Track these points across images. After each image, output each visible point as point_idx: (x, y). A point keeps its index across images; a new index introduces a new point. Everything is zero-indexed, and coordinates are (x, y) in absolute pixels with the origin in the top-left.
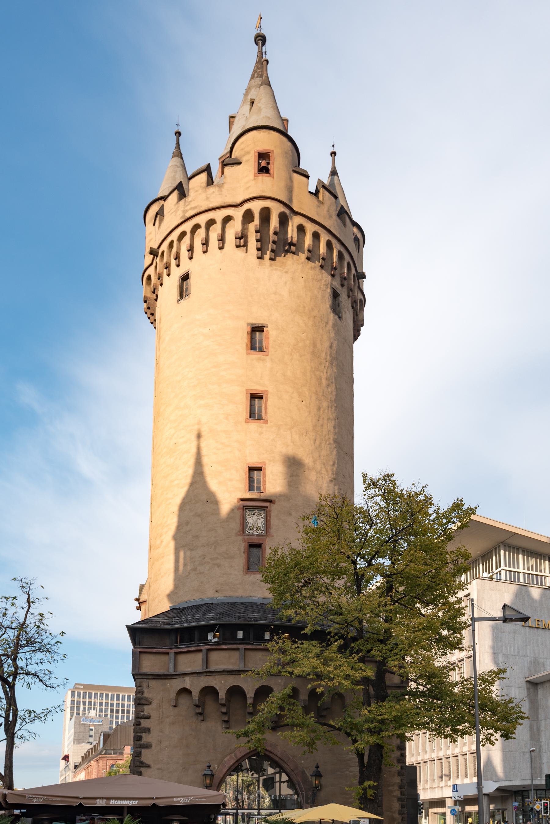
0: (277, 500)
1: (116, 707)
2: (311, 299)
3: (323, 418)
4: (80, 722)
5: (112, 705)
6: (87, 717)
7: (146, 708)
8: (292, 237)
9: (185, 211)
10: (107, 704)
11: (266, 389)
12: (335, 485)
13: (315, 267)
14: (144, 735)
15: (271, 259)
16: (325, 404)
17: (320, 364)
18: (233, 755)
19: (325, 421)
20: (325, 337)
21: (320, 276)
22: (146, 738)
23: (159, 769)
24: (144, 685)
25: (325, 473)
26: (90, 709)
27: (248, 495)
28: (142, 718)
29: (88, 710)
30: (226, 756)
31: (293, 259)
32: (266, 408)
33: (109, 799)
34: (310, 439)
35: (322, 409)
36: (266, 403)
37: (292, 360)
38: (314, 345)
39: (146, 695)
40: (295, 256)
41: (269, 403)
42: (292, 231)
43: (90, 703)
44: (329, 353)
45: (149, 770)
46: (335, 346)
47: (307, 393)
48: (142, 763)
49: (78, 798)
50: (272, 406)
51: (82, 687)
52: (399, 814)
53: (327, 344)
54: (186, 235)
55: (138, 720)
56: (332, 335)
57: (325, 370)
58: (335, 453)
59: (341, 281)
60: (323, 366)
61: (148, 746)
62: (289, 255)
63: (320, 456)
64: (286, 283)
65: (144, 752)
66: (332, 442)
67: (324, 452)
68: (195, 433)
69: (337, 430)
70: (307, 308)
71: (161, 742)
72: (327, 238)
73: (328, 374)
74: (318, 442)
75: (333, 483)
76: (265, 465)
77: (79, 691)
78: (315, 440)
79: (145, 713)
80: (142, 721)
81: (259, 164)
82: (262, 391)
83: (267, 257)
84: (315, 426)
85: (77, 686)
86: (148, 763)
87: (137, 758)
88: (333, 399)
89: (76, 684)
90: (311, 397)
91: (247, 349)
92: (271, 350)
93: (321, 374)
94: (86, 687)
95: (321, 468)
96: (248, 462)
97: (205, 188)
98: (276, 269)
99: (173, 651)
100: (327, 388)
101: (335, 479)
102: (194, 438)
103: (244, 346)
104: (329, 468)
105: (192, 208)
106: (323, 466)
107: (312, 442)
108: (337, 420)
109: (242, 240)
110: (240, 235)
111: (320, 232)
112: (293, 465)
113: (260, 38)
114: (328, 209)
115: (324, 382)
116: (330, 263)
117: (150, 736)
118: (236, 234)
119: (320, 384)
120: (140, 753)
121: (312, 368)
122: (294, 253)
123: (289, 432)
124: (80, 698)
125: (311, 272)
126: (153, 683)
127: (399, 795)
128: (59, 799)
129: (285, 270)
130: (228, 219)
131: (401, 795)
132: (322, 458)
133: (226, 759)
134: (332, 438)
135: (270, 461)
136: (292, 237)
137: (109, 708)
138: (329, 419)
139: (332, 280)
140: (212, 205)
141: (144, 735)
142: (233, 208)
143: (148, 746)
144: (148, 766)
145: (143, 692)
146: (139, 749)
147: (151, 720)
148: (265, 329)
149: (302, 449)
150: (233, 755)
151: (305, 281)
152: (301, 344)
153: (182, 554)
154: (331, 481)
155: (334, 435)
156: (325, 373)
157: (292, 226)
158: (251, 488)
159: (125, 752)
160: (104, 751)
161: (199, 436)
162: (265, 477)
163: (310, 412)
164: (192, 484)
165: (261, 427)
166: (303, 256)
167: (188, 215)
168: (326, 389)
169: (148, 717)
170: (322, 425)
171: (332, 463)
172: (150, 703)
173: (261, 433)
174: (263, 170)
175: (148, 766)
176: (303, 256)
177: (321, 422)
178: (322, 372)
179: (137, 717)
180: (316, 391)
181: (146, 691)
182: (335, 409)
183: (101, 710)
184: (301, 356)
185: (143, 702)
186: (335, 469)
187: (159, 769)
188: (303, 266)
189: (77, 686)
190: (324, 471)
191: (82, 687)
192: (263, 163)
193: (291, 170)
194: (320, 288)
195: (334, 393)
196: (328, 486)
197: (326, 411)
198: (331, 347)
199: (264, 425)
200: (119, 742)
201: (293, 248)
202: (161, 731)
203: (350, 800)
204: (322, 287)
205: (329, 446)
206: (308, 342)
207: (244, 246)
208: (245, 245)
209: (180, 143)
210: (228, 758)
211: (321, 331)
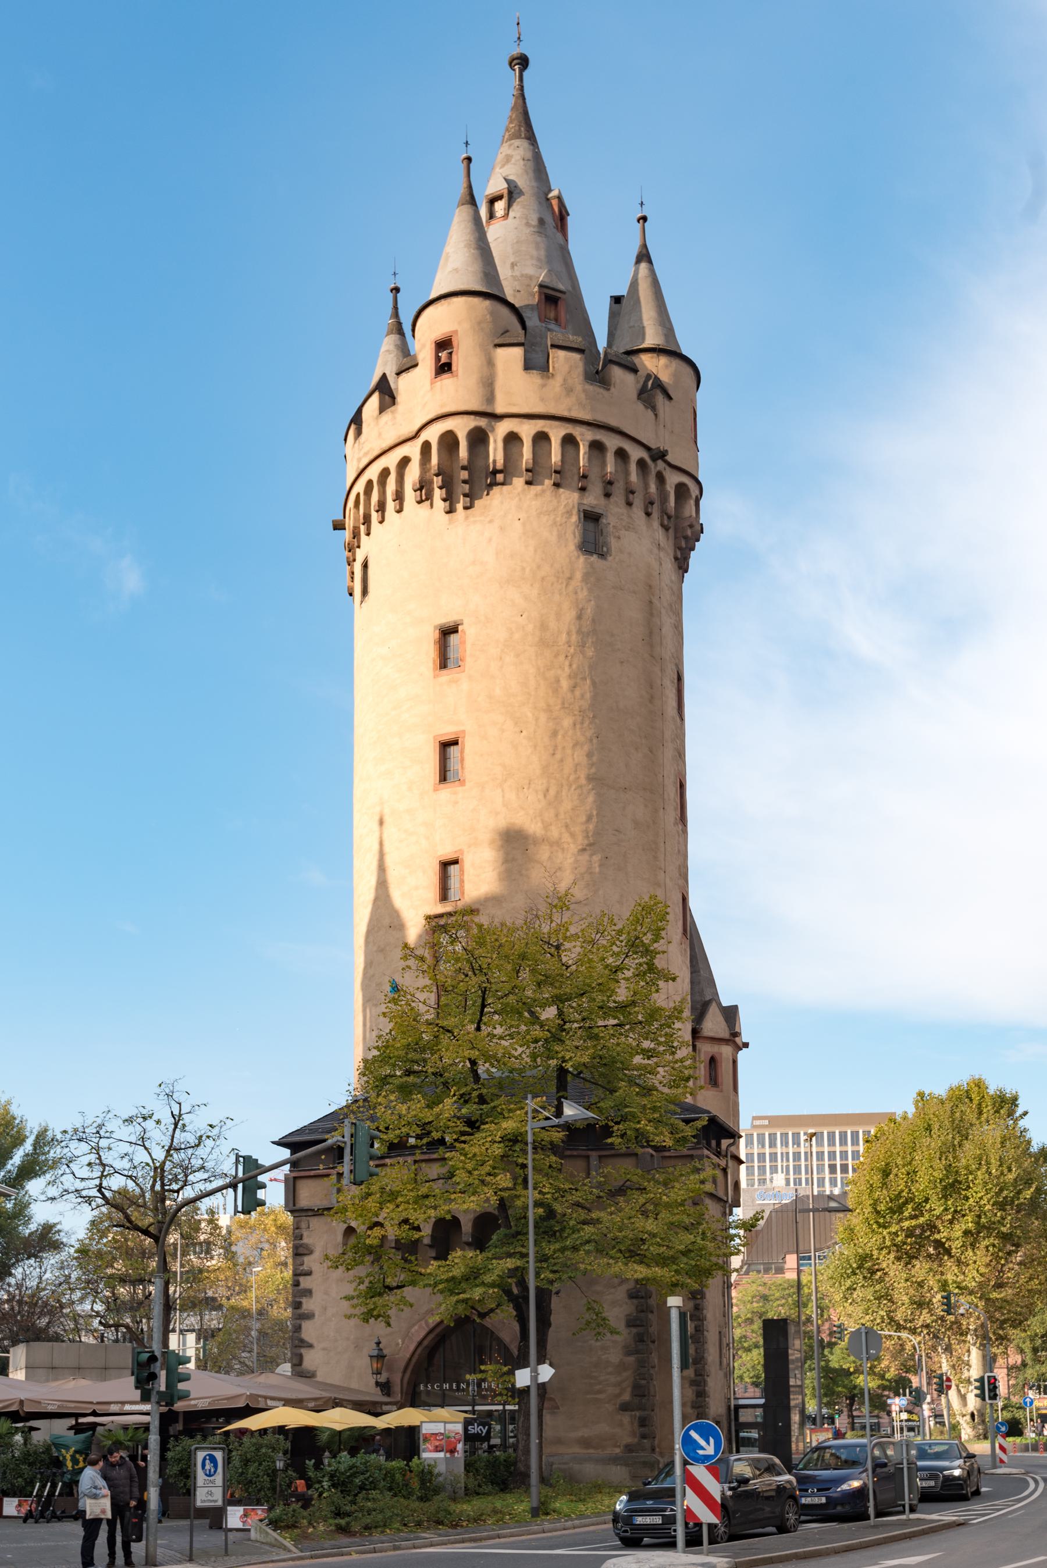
0: (481, 908)
1: (841, 1159)
2: (535, 551)
3: (564, 748)
4: (753, 1200)
5: (832, 1155)
6: (767, 1190)
7: (306, 1259)
8: (494, 461)
9: (359, 460)
10: (820, 1155)
11: (462, 728)
12: (591, 855)
13: (543, 491)
14: (304, 1300)
15: (466, 508)
16: (567, 722)
17: (556, 656)
18: (423, 1322)
19: (569, 751)
20: (566, 605)
21: (555, 502)
22: (308, 1305)
23: (324, 1349)
24: (303, 1225)
25: (570, 840)
26: (774, 1170)
27: (440, 909)
28: (300, 1275)
29: (771, 1173)
30: (414, 1325)
31: (501, 494)
32: (462, 760)
33: (123, 1403)
34: (537, 792)
35: (561, 733)
36: (462, 752)
37: (502, 667)
38: (543, 626)
39: (305, 1240)
40: (505, 487)
41: (467, 751)
42: (495, 449)
43: (773, 1157)
44: (574, 630)
45: (312, 1352)
46: (589, 612)
47: (530, 715)
48: (302, 1341)
49: (91, 1403)
50: (471, 758)
51: (766, 1122)
52: (693, 1407)
53: (570, 615)
54: (389, 473)
55: (297, 1278)
56: (583, 594)
57: (567, 663)
58: (591, 799)
59: (605, 488)
60: (562, 658)
61: (309, 1316)
62: (496, 490)
63: (557, 816)
64: (490, 540)
65: (306, 1325)
66: (583, 781)
67: (567, 805)
68: (377, 818)
69: (595, 759)
70: (528, 570)
71: (325, 1309)
72: (562, 433)
73: (574, 666)
74: (552, 792)
75: (589, 852)
76: (462, 854)
77: (761, 1131)
78: (548, 790)
79: (305, 1267)
80: (301, 1279)
81: (438, 359)
82: (456, 733)
83: (460, 506)
84: (545, 768)
85: (757, 1123)
86: (310, 1341)
87: (296, 1334)
88: (585, 704)
89: (755, 1118)
90: (537, 719)
91: (435, 669)
92: (469, 661)
93: (559, 672)
94: (775, 1121)
95: (561, 834)
96: (439, 854)
97: (377, 418)
98: (475, 522)
99: (334, 1172)
100: (572, 691)
101: (590, 845)
102: (375, 826)
103: (431, 665)
104: (577, 829)
105: (366, 454)
106: (563, 830)
107: (541, 796)
108: (595, 741)
109: (424, 490)
110: (418, 486)
111: (546, 430)
112: (514, 844)
113: (515, 62)
114: (565, 380)
115: (565, 684)
116: (575, 471)
117: (312, 1301)
118: (414, 485)
119: (556, 691)
120: (300, 1327)
121: (539, 669)
122: (503, 484)
123: (499, 790)
124: (763, 1146)
125: (536, 504)
126: (315, 1222)
127: (692, 1375)
128: (73, 1405)
129: (488, 519)
130: (405, 461)
131: (696, 1375)
132: (562, 816)
133: (413, 1330)
134: (583, 776)
135: (469, 847)
136: (494, 461)
137: (827, 1163)
138: (575, 745)
139: (581, 498)
140: (386, 445)
141: (304, 1300)
142: (409, 443)
143: (309, 1316)
144: (311, 1346)
145: (302, 1236)
146: (298, 1321)
147: (313, 1276)
148: (460, 628)
149: (522, 813)
150: (423, 1322)
151: (524, 524)
152: (517, 636)
153: (368, 1011)
154: (584, 850)
155: (590, 769)
156: (567, 669)
157: (495, 441)
158: (444, 897)
159: (786, 1266)
160: (745, 1267)
161: (381, 823)
162: (463, 874)
163: (535, 746)
164: (376, 900)
165: (455, 793)
166: (519, 482)
167: (362, 466)
168: (569, 695)
169: (309, 1273)
170: (562, 761)
171: (584, 819)
172: (311, 1252)
173: (456, 803)
174: (444, 368)
175: (311, 1346)
176: (519, 482)
177: (558, 756)
178: (561, 668)
179: (296, 1274)
180: (549, 706)
181: (305, 1234)
182: (591, 723)
183: (797, 1169)
184: (518, 656)
185: (301, 1250)
186: (591, 827)
187: (324, 1349)
188: (520, 499)
189: (757, 1123)
190: (566, 838)
191: (766, 1122)
192: (443, 355)
193: (491, 346)
194: (555, 523)
195: (588, 696)
196: (576, 861)
197: (570, 733)
198: (579, 617)
199: (460, 788)
200: (775, 1247)
201: (500, 477)
202: (326, 1293)
203: (598, 1387)
204: (558, 519)
205: (578, 791)
206: (530, 627)
207: (427, 499)
208: (429, 497)
209: (399, 306)
210: (416, 1327)
211: (557, 598)
